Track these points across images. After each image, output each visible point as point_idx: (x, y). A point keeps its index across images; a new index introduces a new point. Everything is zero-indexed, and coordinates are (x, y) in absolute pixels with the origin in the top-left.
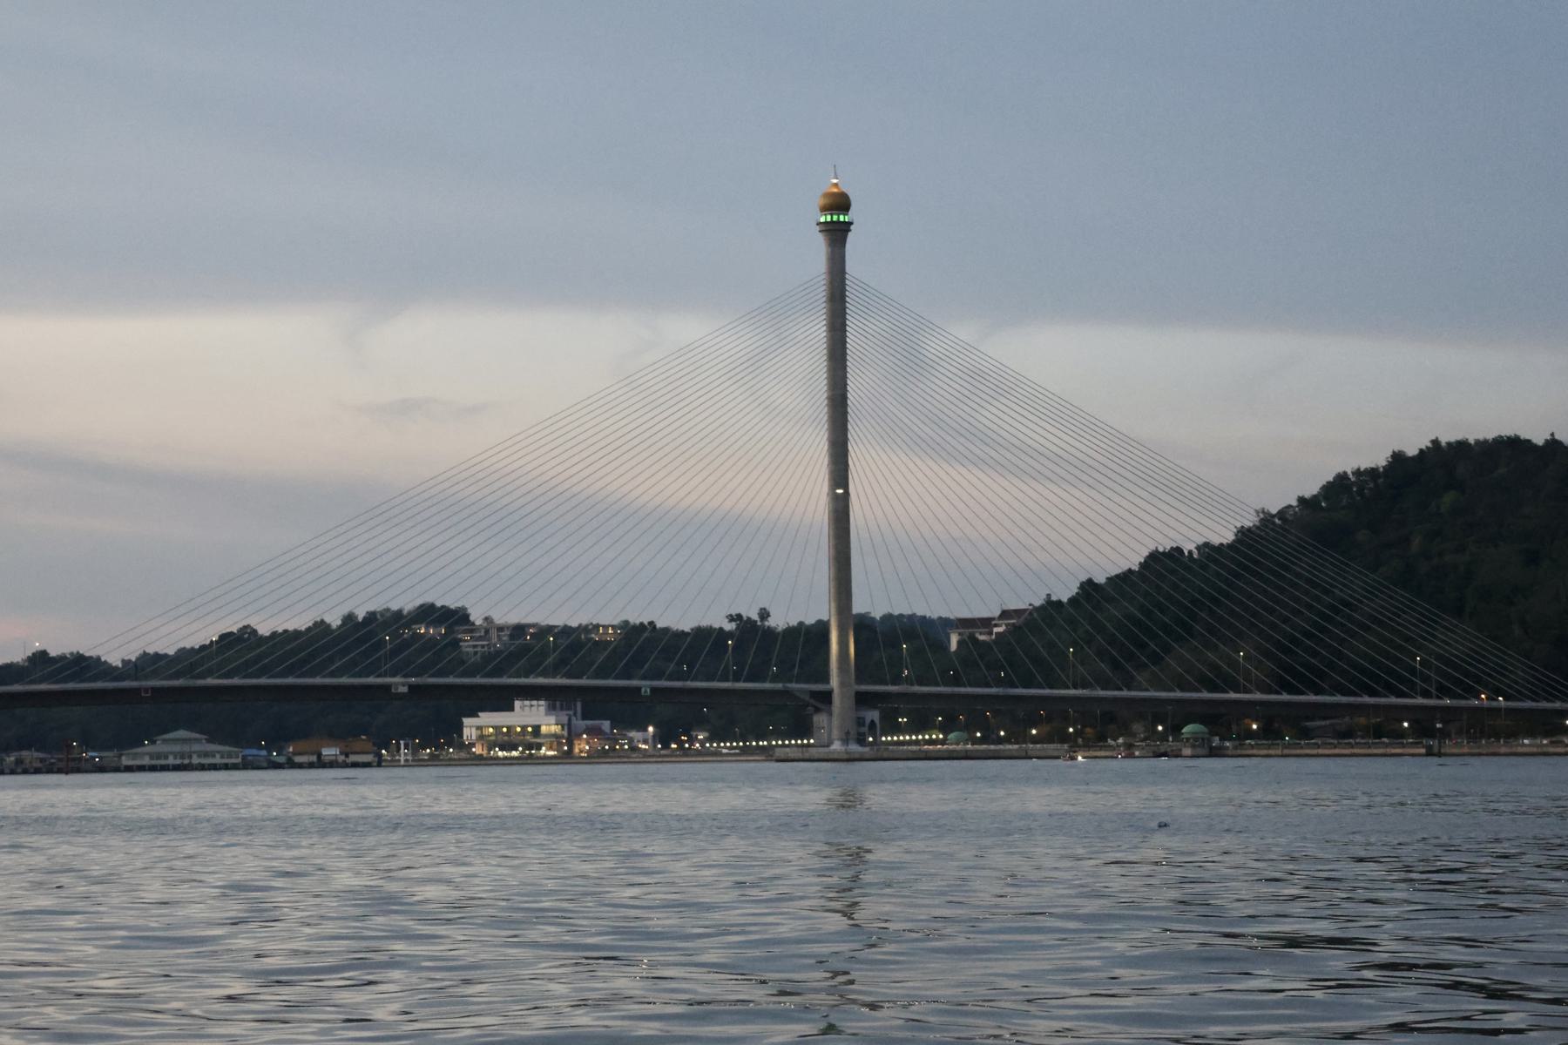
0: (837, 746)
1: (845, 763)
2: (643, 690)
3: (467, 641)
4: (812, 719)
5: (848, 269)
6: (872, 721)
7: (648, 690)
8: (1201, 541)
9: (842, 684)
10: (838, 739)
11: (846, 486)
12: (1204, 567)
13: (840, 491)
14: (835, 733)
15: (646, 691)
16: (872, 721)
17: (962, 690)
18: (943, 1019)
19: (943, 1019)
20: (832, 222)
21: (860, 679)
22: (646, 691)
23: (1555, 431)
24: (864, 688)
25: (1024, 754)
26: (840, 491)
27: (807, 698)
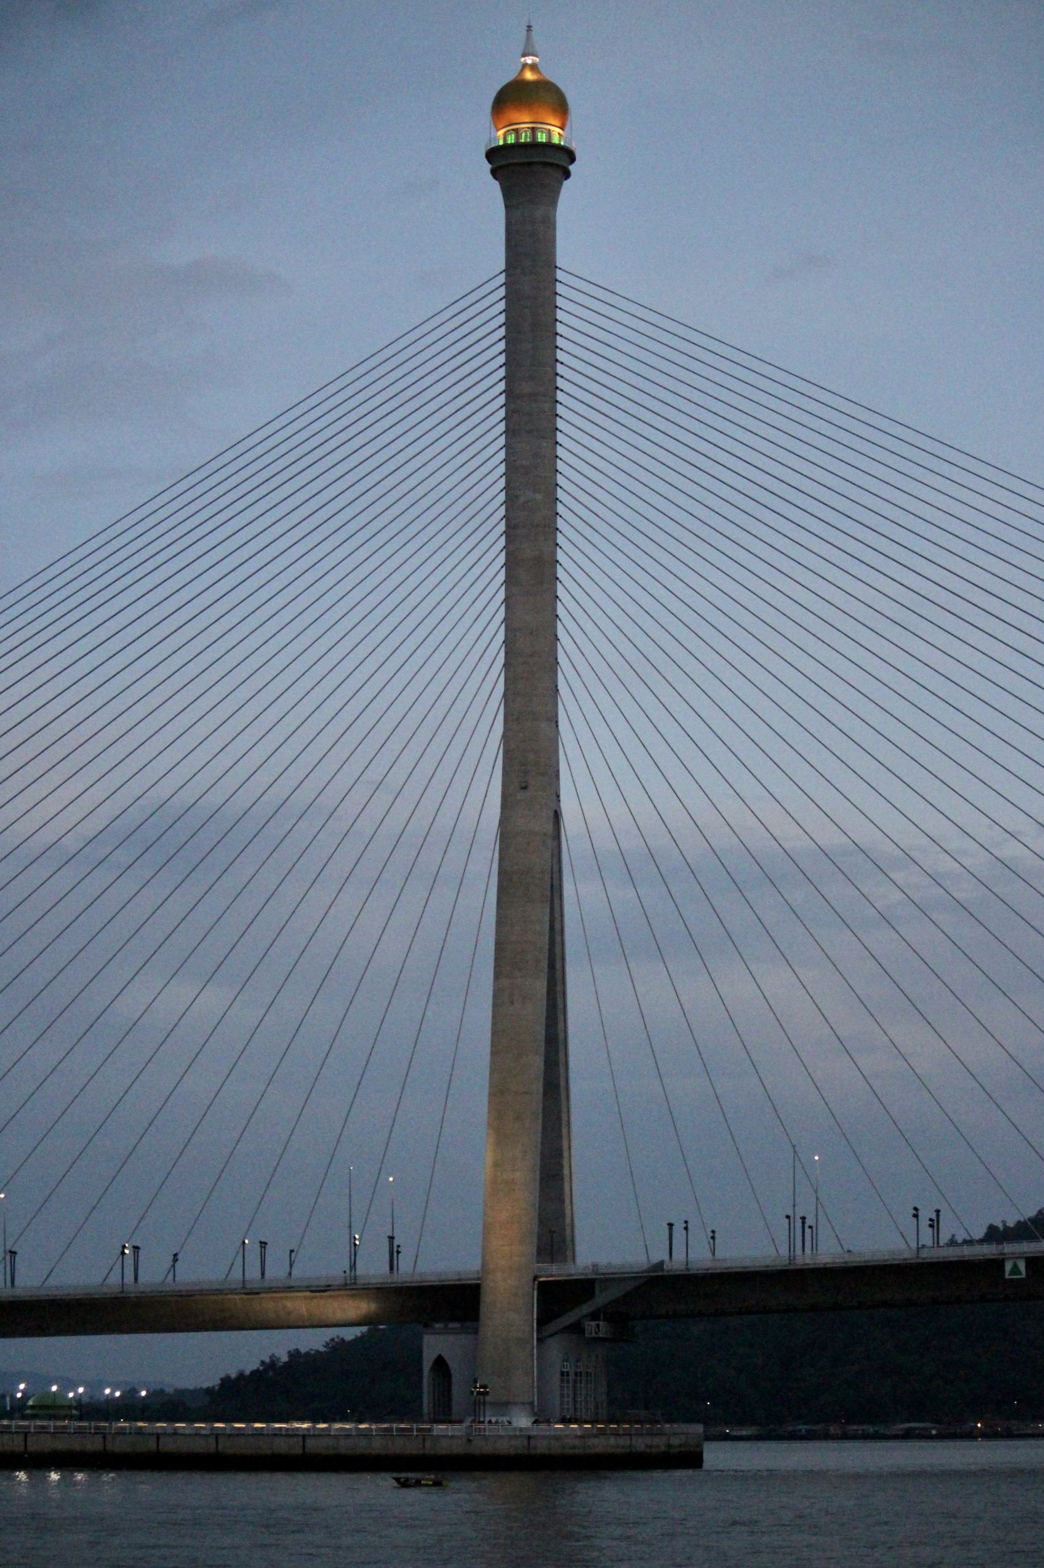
2: (1008, 1266)
7: (1022, 1266)
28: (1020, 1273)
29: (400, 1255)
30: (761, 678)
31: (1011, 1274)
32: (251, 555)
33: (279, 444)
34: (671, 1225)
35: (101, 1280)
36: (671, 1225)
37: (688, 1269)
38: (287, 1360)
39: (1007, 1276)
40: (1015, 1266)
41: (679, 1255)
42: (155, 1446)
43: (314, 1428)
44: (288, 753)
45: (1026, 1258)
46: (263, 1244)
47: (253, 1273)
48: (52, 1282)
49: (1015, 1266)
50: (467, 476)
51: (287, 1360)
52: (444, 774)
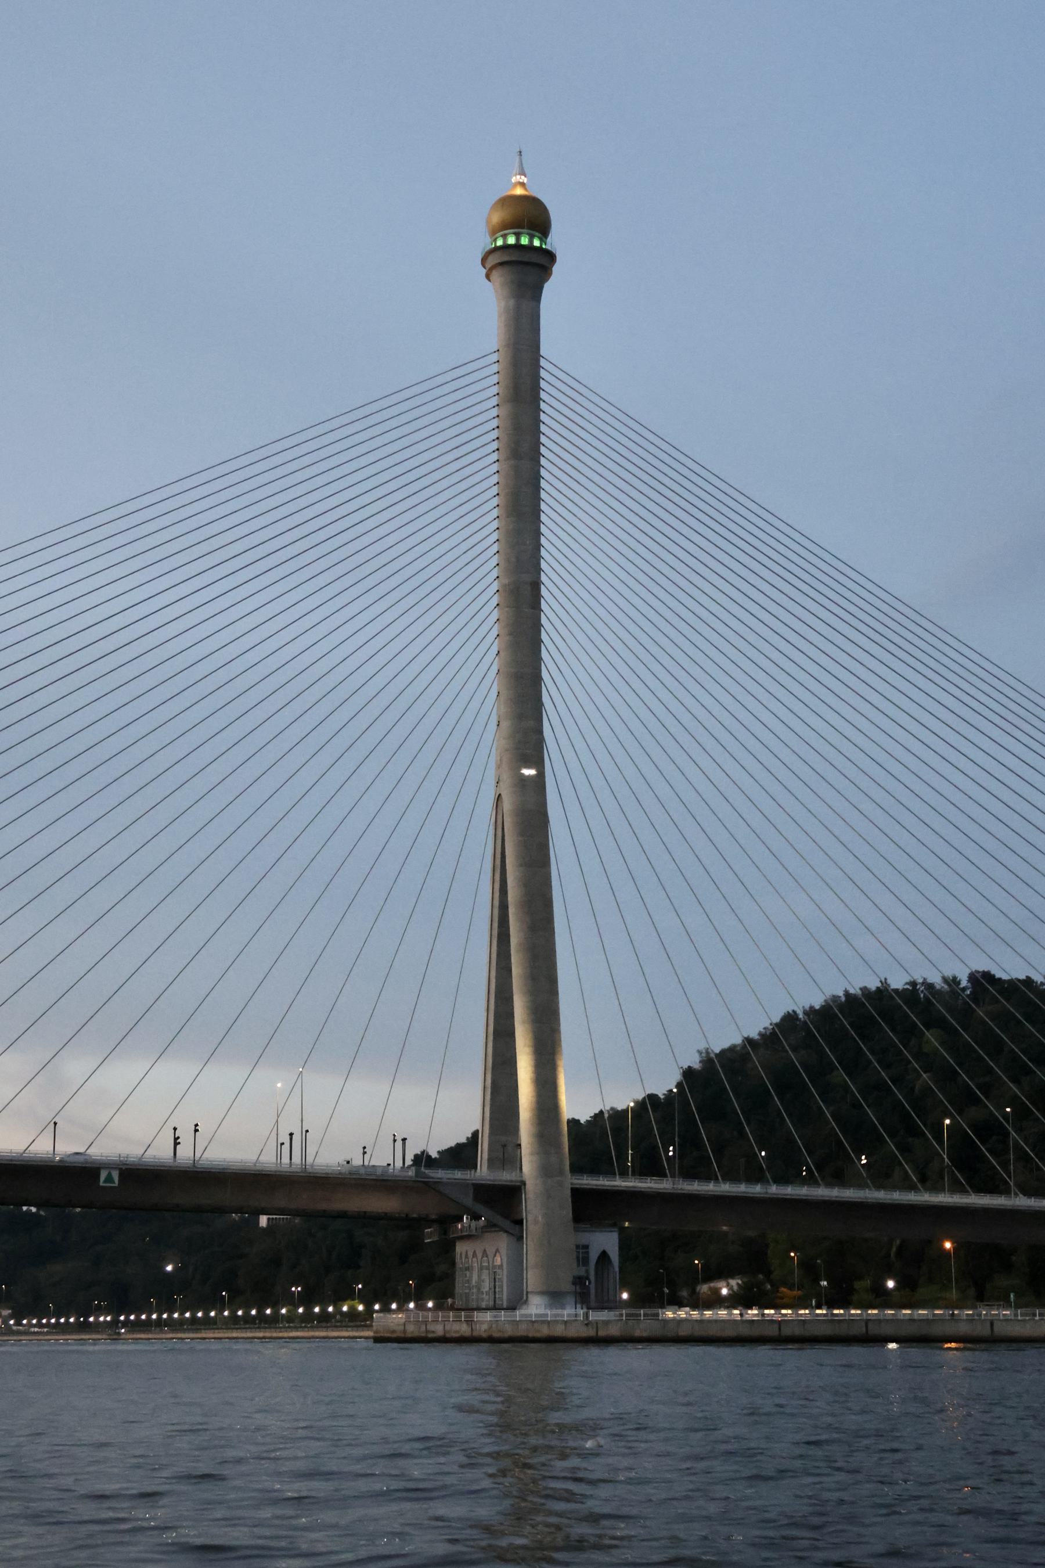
0: (536, 1307)
1: (543, 1346)
2: (103, 1175)
3: (622, 1529)
4: (455, 1246)
5: (546, 348)
6: (604, 1256)
7: (115, 1175)
8: (981, 965)
9: (546, 1171)
10: (542, 1293)
11: (538, 762)
12: (965, 1014)
13: (529, 772)
14: (532, 1278)
15: (109, 1178)
16: (604, 1256)
17: (710, 1188)
18: (279, 1512)
19: (279, 1512)
20: (518, 246)
21: (577, 1169)
22: (109, 1178)
23: (888, 977)
24: (630, 1173)
25: (986, 1331)
26: (529, 772)
27: (468, 1201)
28: (114, 1183)
29: (178, 1146)
30: (441, 578)
31: (105, 1182)
32: (633, 526)
33: (365, 506)
34: (291, 1135)
35: (255, 1158)
36: (291, 1135)
37: (194, 1166)
38: (261, 1216)
39: (101, 1184)
40: (110, 1175)
41: (297, 1159)
42: (864, 1329)
43: (763, 1315)
44: (609, 713)
45: (120, 1169)
46: (404, 1140)
47: (286, 1160)
48: (150, 1153)
49: (110, 1175)
50: (479, 437)
51: (261, 1216)
52: (590, 708)
